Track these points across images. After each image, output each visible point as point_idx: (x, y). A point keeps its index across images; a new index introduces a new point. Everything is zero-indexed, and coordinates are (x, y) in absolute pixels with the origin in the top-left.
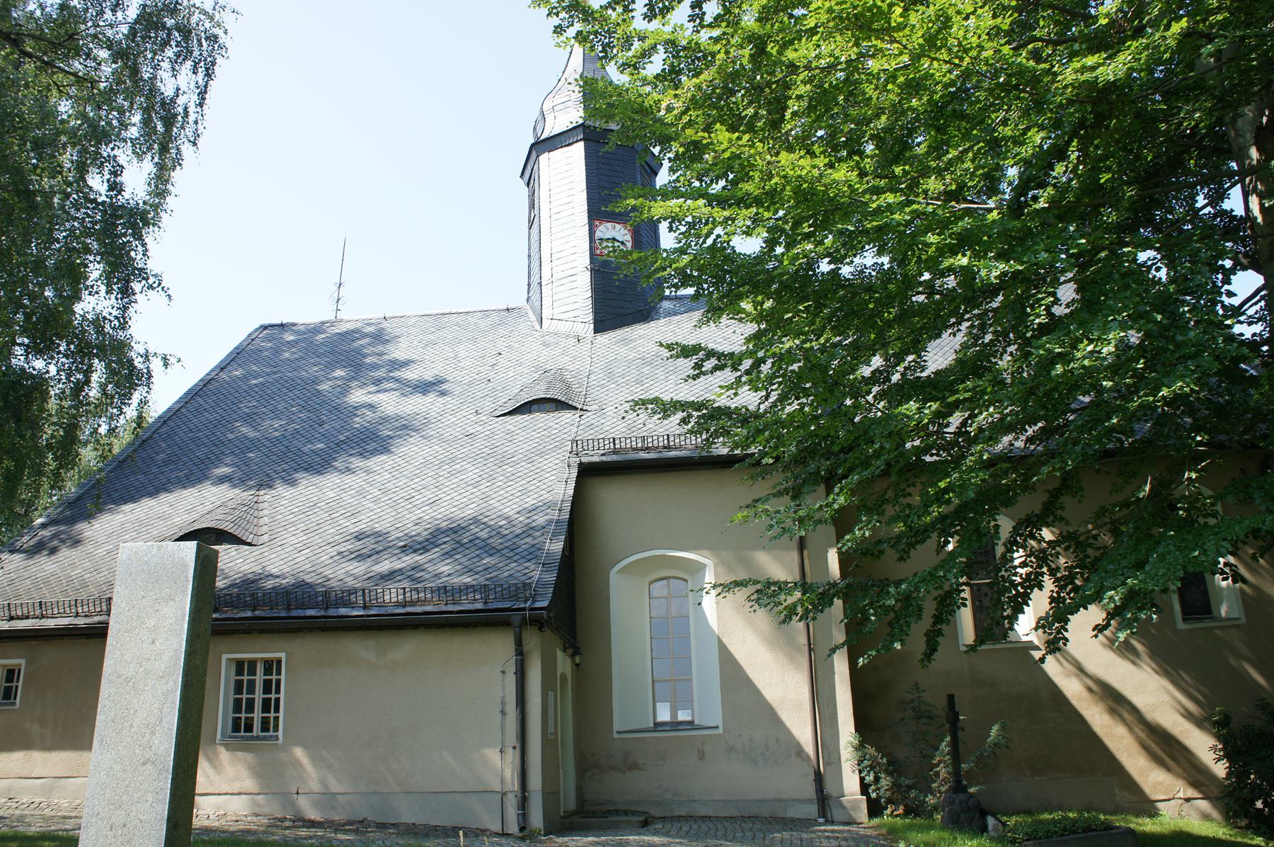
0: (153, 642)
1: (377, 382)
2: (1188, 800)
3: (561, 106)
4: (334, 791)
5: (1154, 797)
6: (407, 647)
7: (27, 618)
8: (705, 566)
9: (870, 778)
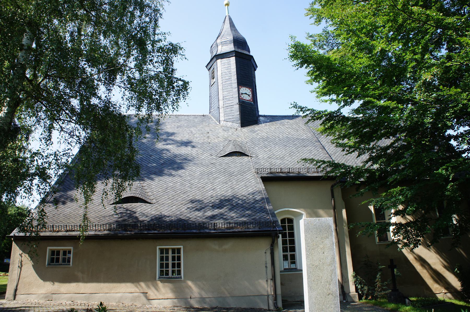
0: (324, 253)
1: (165, 140)
2: (445, 293)
3: (224, 43)
4: (204, 297)
5: (435, 292)
6: (229, 244)
7: (74, 231)
8: (302, 214)
9: (359, 287)
